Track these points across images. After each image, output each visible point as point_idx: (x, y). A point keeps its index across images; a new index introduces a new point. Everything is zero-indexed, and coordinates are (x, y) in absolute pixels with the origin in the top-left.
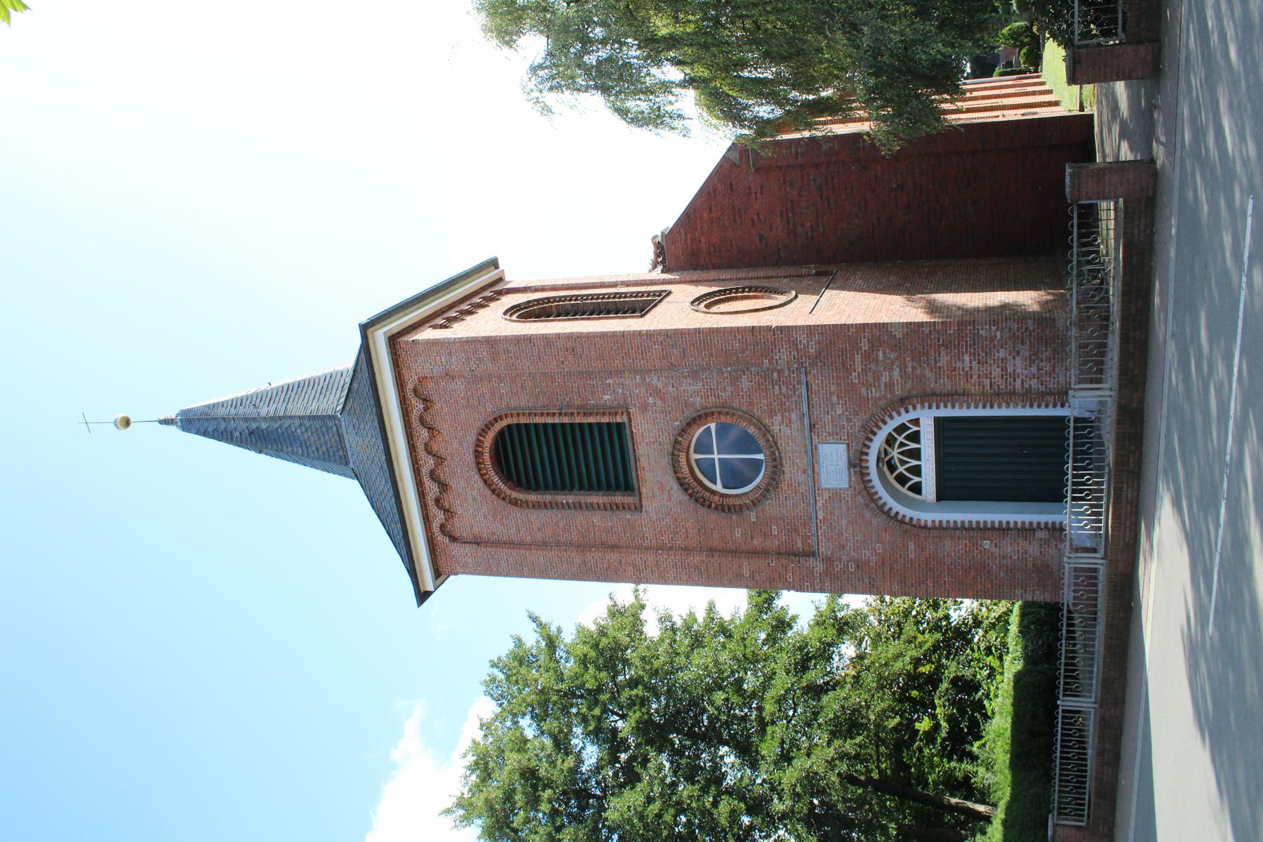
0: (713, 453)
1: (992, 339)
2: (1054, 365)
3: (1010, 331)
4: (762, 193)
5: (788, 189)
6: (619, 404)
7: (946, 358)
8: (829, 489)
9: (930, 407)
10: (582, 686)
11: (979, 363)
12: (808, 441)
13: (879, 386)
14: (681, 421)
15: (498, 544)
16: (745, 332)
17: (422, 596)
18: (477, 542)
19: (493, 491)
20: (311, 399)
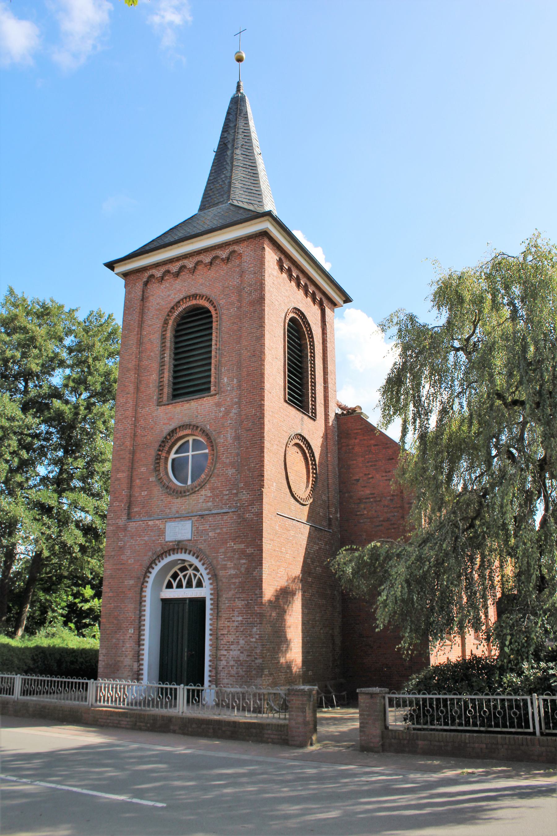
0: (193, 451)
1: (251, 635)
2: (234, 676)
3: (256, 647)
4: (386, 480)
5: (389, 498)
6: (221, 388)
7: (240, 605)
8: (165, 528)
9: (211, 594)
10: (90, 373)
11: (237, 626)
12: (195, 514)
13: (225, 561)
14: (209, 430)
15: (142, 313)
16: (261, 470)
17: (111, 265)
18: (144, 299)
19: (173, 308)
20: (244, 183)
